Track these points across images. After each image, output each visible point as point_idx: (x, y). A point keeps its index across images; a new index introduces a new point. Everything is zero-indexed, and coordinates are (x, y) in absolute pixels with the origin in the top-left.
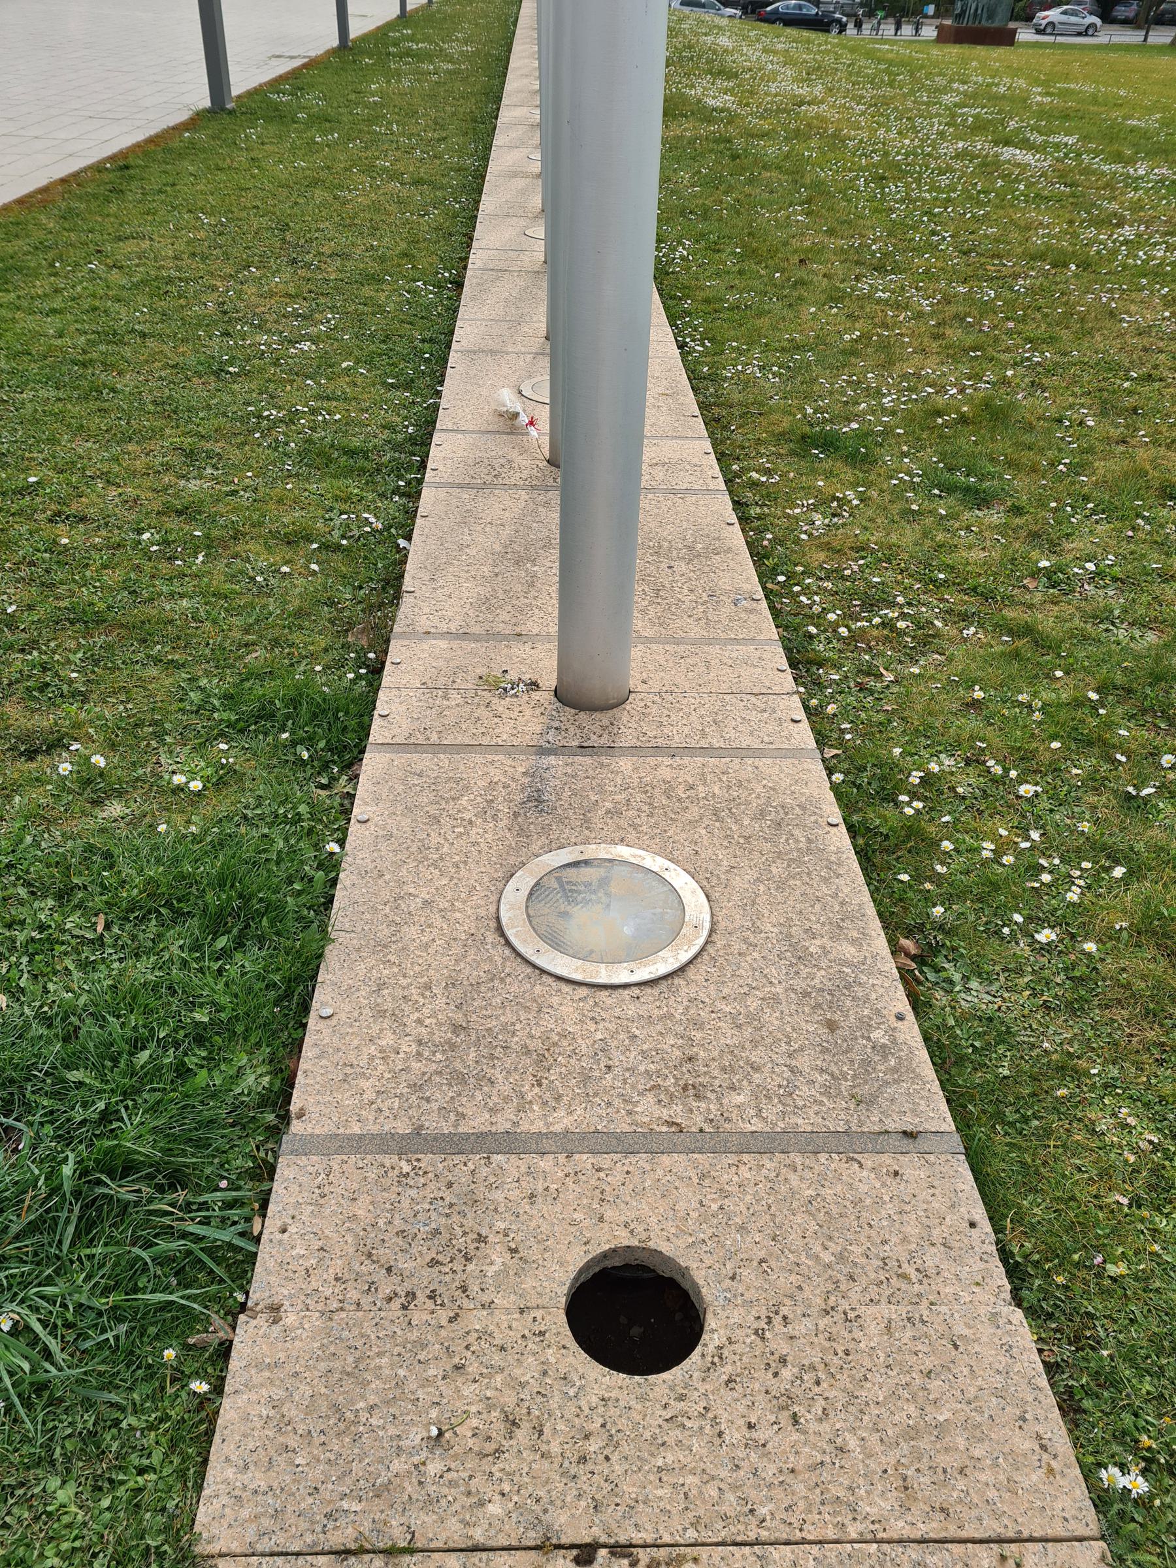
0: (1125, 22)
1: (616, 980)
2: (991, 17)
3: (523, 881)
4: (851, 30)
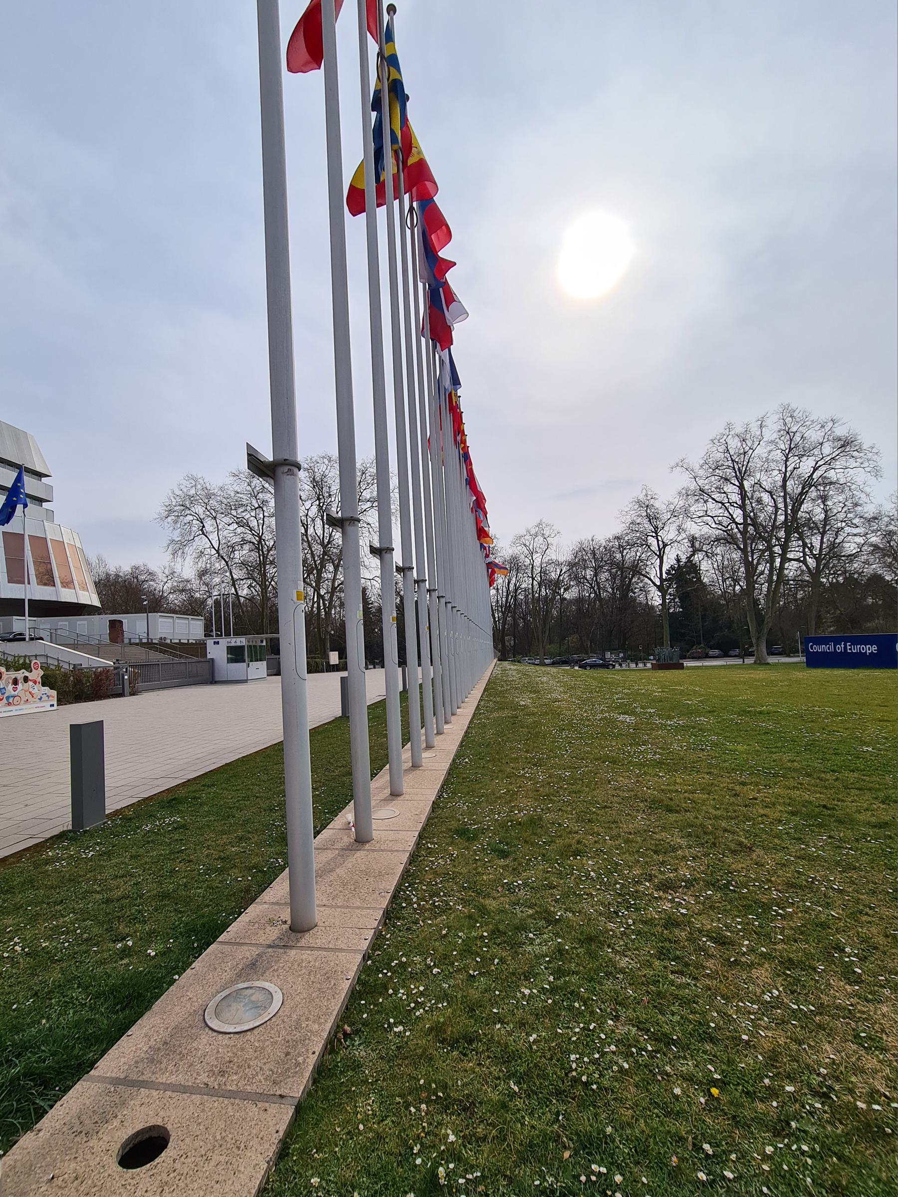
0: (735, 656)
1: (228, 1031)
2: (671, 659)
3: (273, 1009)
4: (617, 667)
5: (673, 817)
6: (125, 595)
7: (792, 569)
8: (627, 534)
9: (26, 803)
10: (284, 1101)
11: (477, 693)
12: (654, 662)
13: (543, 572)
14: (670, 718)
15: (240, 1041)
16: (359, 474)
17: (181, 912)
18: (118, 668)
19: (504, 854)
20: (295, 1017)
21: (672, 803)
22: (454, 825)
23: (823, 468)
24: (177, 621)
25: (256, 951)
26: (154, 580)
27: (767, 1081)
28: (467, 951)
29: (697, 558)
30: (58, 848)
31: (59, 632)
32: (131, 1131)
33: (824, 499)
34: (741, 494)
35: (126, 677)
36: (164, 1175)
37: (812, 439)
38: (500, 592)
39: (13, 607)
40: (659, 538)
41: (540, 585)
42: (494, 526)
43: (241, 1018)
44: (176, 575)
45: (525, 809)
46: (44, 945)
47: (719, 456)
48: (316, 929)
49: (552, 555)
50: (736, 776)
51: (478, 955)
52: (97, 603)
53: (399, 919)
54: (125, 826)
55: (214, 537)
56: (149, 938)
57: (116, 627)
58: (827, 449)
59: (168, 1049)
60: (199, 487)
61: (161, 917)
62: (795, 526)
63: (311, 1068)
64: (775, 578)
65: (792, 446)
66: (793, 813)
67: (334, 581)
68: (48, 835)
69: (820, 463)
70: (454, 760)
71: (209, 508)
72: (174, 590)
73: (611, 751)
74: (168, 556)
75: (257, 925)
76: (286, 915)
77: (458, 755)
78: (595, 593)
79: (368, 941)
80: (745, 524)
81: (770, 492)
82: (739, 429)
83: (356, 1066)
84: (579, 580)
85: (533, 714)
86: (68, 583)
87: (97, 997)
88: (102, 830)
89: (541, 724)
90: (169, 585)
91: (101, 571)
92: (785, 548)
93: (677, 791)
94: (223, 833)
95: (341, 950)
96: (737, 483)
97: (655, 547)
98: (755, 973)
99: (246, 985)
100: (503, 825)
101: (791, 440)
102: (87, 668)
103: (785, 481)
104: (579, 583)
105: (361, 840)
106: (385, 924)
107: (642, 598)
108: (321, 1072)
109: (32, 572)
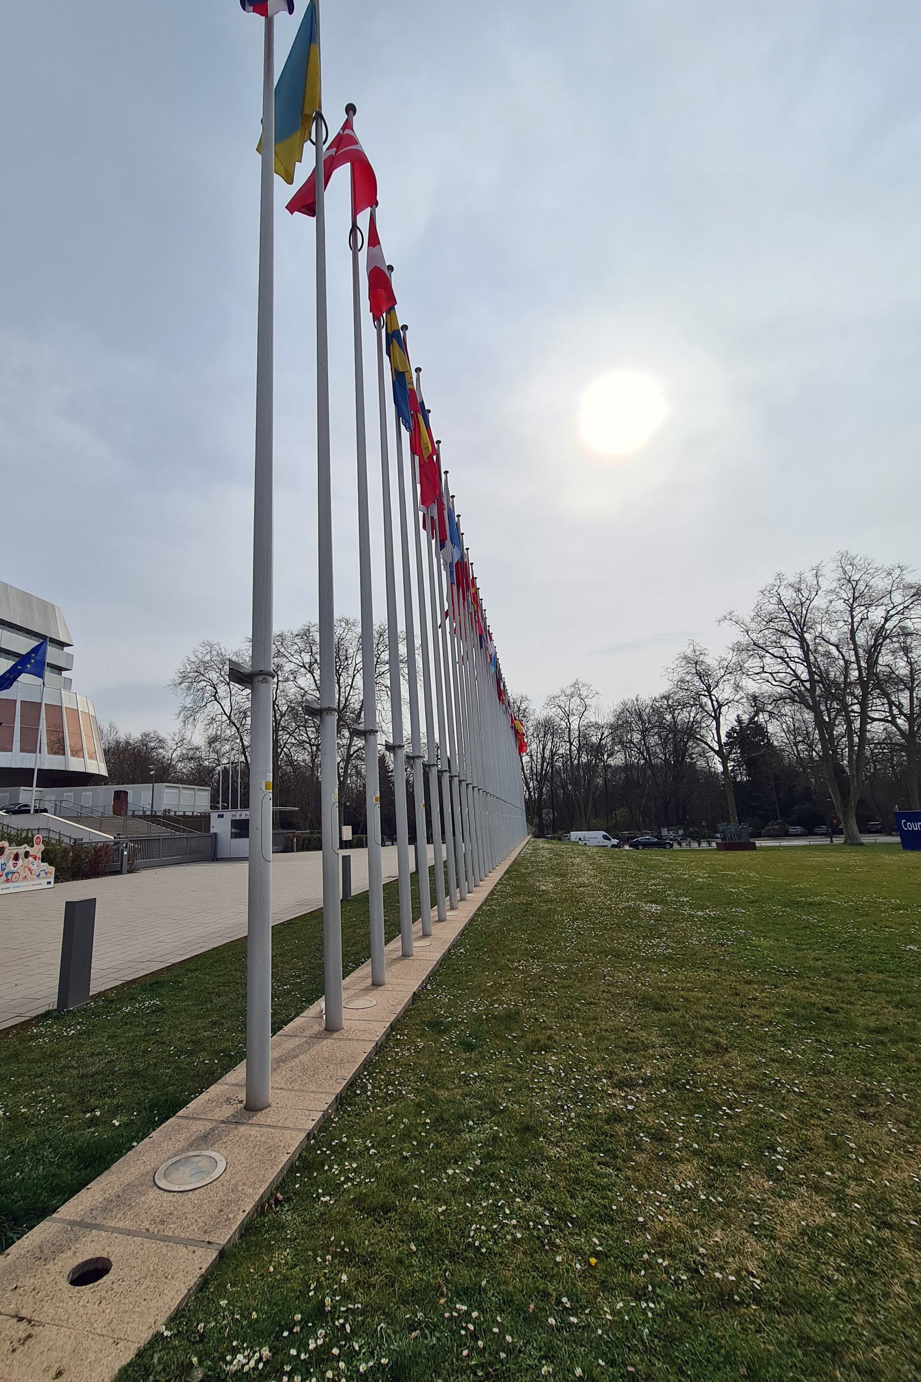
0: (822, 834)
3: (215, 1175)
5: (657, 1016)
6: (134, 763)
7: (876, 729)
8: (675, 693)
9: (16, 982)
10: (210, 1246)
11: (495, 876)
12: (719, 841)
13: (583, 736)
14: (702, 908)
15: (181, 1198)
16: (376, 635)
17: (148, 1089)
18: (119, 843)
19: (469, 1047)
20: (233, 1181)
21: (663, 1002)
22: (429, 1016)
23: (896, 619)
24: (183, 792)
25: (209, 1125)
26: (163, 748)
27: (646, 1256)
28: (407, 1135)
29: (762, 718)
30: (43, 1026)
31: (64, 804)
32: (80, 1260)
33: (906, 650)
34: (802, 647)
35: (125, 853)
36: (103, 1294)
37: (879, 588)
38: (535, 758)
39: (21, 777)
40: (714, 698)
41: (579, 750)
42: (513, 690)
43: (183, 1179)
44: (185, 742)
45: (508, 1001)
46: (23, 1110)
47: (772, 607)
48: (268, 1109)
49: (591, 717)
50: (747, 974)
51: (415, 1138)
52: (104, 773)
53: (350, 1105)
54: (106, 1007)
55: (226, 704)
56: (114, 1111)
57: (120, 797)
58: (897, 598)
59: (121, 1201)
60: (214, 653)
61: (129, 1093)
62: (874, 682)
63: (239, 1223)
64: (856, 740)
65: (857, 595)
66: (789, 1016)
67: (350, 746)
68: (34, 1014)
69: (891, 613)
70: (449, 950)
71: (223, 673)
72: (182, 758)
73: (618, 943)
74: (178, 724)
75: (214, 1103)
76: (242, 1096)
77: (456, 944)
78: (645, 759)
79: (314, 1122)
80: (812, 680)
81: (837, 646)
82: (792, 579)
83: (282, 1227)
84: (626, 745)
85: (551, 901)
86: (78, 752)
87: (64, 1157)
88: (85, 1010)
89: (555, 911)
90: (178, 752)
91: (112, 738)
92: (863, 704)
93: (674, 989)
94: (198, 1017)
95: (288, 1128)
96: (796, 636)
97: (709, 707)
98: (681, 1167)
99: (196, 1153)
100: (478, 1019)
101: (854, 589)
102: (87, 843)
103: (853, 632)
104: (624, 748)
105: (331, 1028)
106: (337, 1109)
107: (701, 763)
108: (248, 1229)
109: (45, 740)
